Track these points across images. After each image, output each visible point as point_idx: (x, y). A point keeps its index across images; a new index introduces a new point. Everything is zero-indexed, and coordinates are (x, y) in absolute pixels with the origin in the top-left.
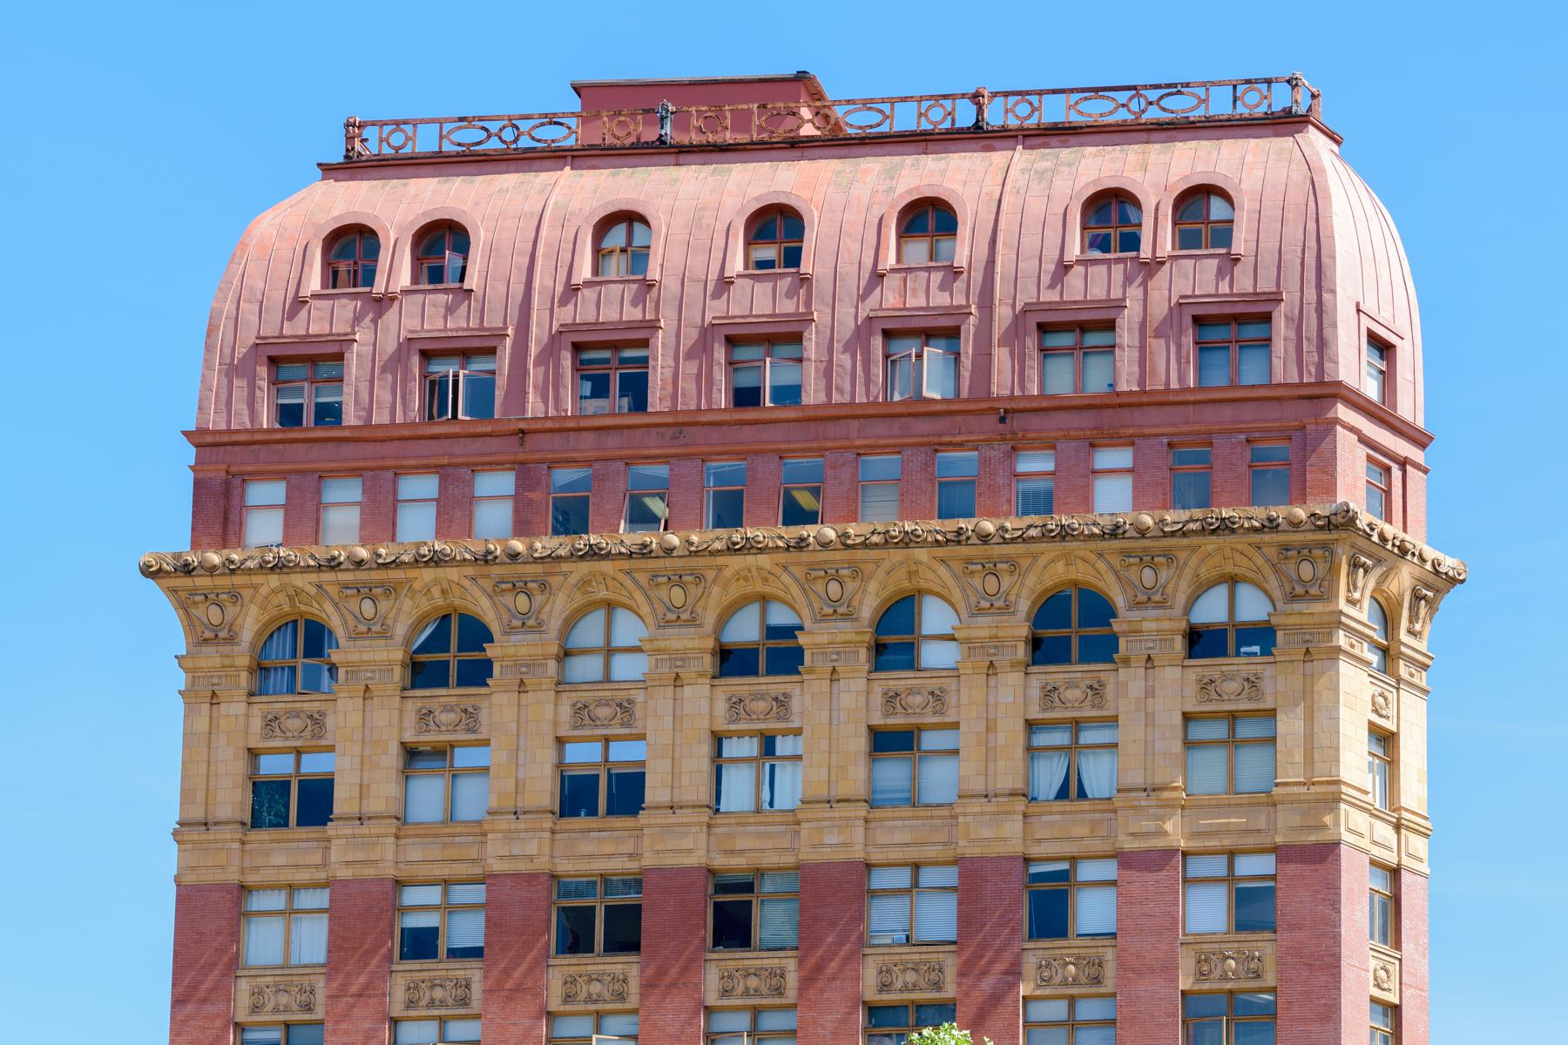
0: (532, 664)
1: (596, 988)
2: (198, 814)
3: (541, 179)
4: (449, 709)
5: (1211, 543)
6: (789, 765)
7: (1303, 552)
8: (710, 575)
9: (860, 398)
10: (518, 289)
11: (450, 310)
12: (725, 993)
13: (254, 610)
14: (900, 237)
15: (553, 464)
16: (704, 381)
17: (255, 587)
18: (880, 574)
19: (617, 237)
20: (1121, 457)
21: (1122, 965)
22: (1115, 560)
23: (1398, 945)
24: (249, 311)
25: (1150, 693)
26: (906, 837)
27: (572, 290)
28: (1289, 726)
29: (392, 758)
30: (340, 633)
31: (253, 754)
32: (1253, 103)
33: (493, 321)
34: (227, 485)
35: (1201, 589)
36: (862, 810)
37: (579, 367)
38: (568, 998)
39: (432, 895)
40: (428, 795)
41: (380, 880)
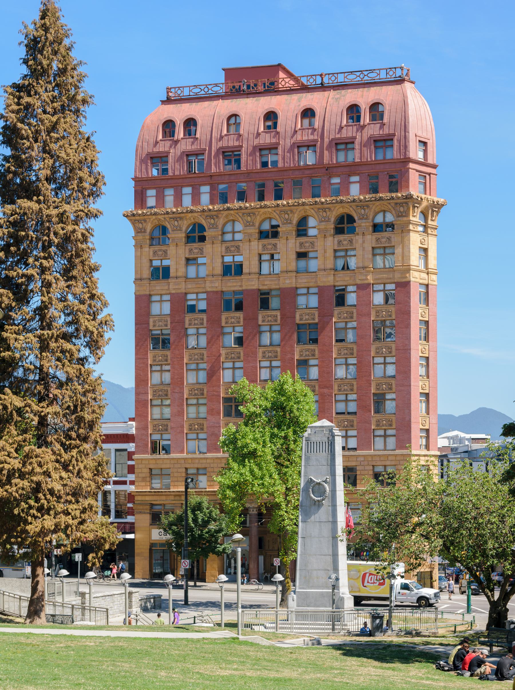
0: (215, 237)
1: (233, 320)
2: (139, 277)
3: (215, 103)
4: (196, 248)
5: (378, 203)
6: (277, 262)
7: (401, 205)
8: (257, 213)
9: (292, 165)
10: (209, 137)
11: (193, 143)
12: (263, 321)
13: (150, 224)
14: (302, 118)
15: (218, 184)
16: (254, 161)
17: (150, 219)
18: (298, 212)
19: (232, 121)
20: (356, 178)
21: (358, 314)
22: (354, 207)
23: (428, 305)
24: (145, 145)
25: (364, 242)
26: (305, 281)
27: (221, 137)
28: (398, 251)
29: (183, 262)
30: (170, 229)
31: (151, 261)
32: (391, 76)
33: (203, 146)
34: (142, 191)
35: (376, 214)
36: (294, 274)
37: (224, 157)
38: (226, 323)
39: (193, 296)
40: (192, 271)
41: (182, 293)
